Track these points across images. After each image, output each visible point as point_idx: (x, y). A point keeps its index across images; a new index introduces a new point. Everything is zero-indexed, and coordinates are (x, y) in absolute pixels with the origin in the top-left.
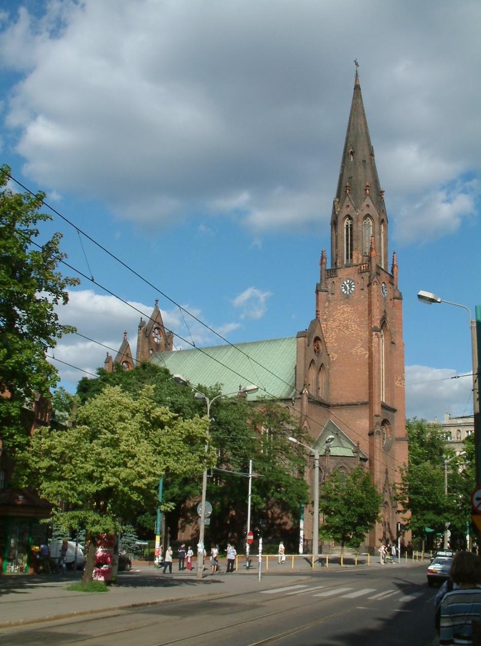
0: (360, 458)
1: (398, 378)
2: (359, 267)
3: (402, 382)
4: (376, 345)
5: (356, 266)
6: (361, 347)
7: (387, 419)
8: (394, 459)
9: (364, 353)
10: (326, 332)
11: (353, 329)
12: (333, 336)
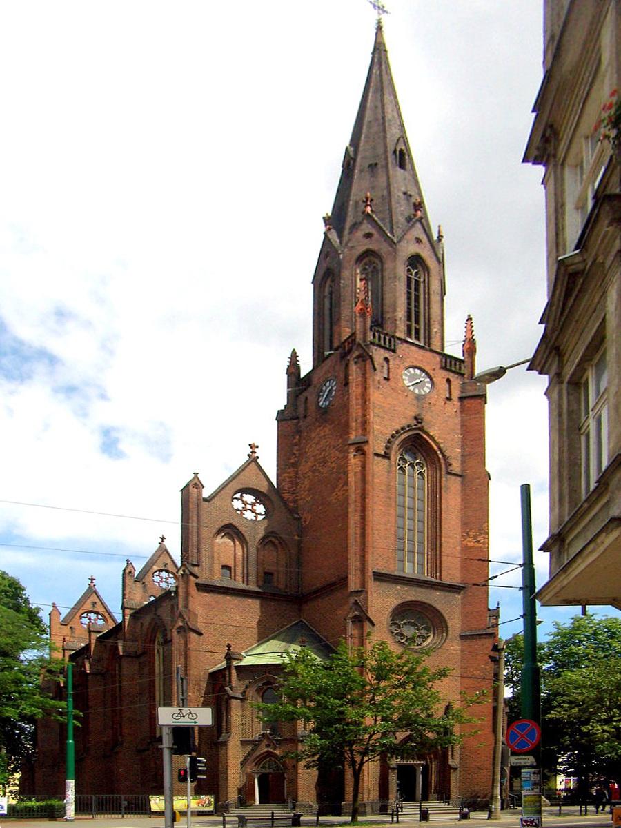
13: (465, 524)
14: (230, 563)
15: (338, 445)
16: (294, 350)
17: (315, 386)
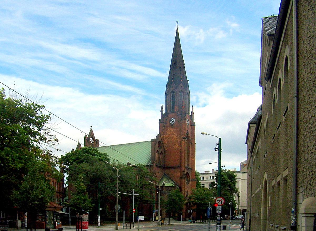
4: (184, 144)
5: (176, 112)
6: (178, 145)
8: (306, 227)
10: (163, 139)
13: (192, 155)
14: (157, 159)
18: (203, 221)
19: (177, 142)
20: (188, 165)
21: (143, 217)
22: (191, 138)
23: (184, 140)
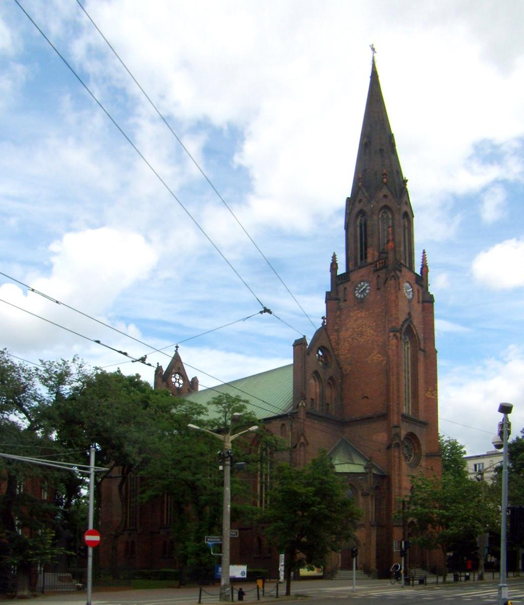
0: (374, 474)
1: (429, 389)
2: (373, 265)
3: (434, 393)
4: (394, 348)
5: (371, 264)
6: (378, 353)
7: (414, 432)
9: (381, 359)
11: (369, 335)
12: (346, 347)
13: (426, 382)
14: (314, 398)
15: (372, 326)
16: (334, 253)
17: (353, 283)
18: (456, 579)
19: (376, 347)
20: (416, 408)
21: (244, 568)
22: (421, 336)
23: (394, 335)
